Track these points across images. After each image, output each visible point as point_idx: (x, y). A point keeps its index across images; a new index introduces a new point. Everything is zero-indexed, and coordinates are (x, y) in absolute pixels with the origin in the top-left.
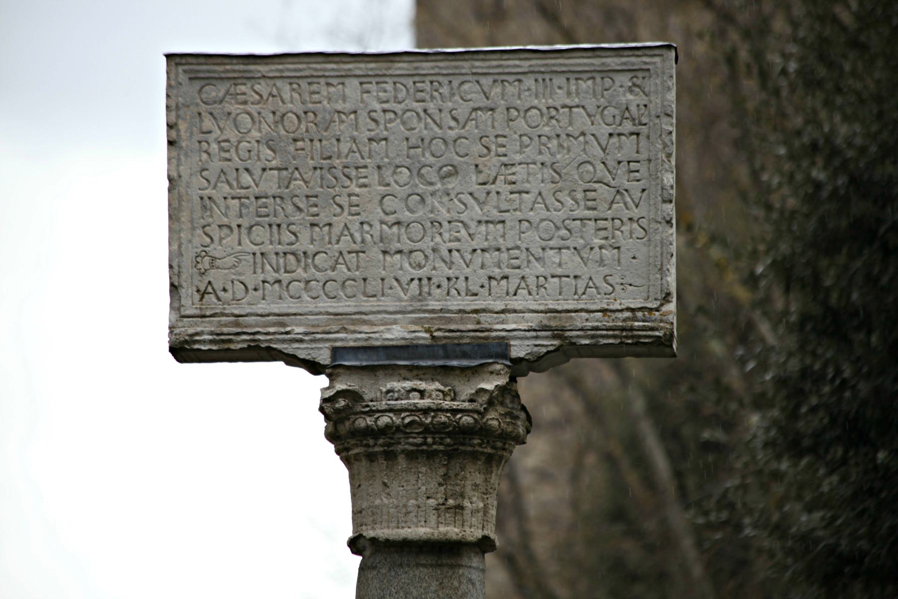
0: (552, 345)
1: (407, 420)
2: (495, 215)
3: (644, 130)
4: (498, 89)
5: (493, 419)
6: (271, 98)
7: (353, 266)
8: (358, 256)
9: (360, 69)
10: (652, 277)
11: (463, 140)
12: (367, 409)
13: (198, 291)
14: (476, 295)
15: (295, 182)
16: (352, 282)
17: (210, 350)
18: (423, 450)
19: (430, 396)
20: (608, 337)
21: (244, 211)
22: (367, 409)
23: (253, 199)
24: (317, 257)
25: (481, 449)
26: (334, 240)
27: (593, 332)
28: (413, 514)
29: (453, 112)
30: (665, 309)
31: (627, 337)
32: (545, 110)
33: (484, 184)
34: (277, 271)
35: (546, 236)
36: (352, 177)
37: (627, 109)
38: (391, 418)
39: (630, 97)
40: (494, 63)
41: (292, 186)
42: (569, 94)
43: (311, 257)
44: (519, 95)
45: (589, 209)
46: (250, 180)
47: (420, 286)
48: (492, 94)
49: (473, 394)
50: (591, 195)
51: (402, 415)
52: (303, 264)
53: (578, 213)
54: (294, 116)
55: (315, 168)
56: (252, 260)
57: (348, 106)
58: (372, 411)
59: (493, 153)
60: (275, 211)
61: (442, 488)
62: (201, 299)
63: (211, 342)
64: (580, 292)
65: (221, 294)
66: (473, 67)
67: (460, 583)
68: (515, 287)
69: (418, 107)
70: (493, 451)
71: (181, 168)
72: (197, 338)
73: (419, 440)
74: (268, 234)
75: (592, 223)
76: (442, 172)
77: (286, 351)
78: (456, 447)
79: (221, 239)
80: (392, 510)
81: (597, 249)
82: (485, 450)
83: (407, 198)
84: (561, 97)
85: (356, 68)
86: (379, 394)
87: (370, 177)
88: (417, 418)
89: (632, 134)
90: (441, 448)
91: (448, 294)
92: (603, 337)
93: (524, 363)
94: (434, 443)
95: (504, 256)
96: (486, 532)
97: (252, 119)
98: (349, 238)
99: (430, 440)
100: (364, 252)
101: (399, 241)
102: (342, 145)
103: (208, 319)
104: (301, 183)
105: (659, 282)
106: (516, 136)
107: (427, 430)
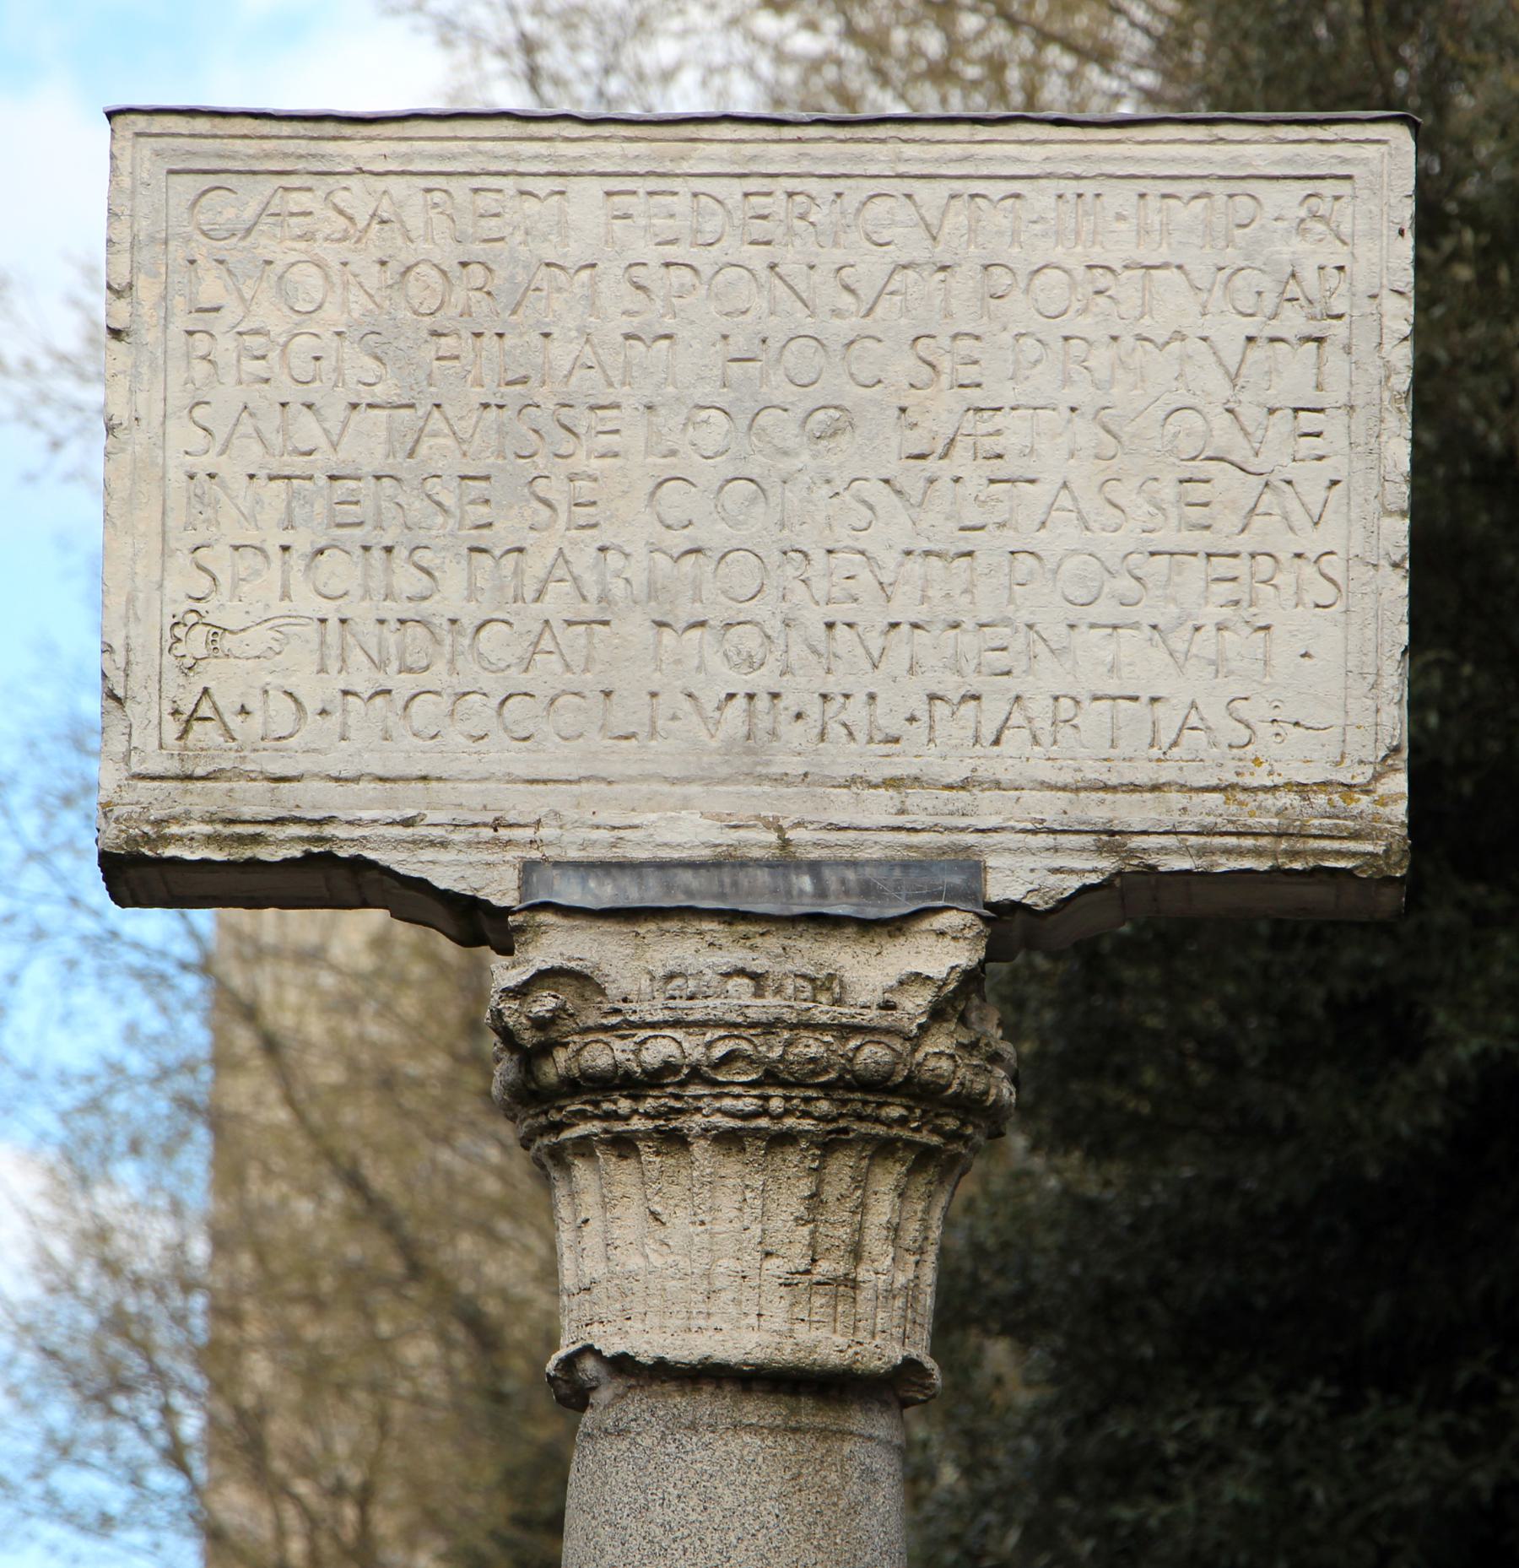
0: (1094, 870)
1: (719, 1051)
2: (947, 537)
3: (1338, 329)
4: (958, 217)
5: (940, 1054)
6: (375, 226)
7: (577, 661)
8: (590, 635)
9: (608, 157)
10: (1353, 705)
11: (869, 343)
12: (614, 1020)
13: (176, 712)
14: (897, 740)
15: (432, 441)
16: (577, 699)
17: (205, 863)
18: (758, 1129)
19: (778, 991)
20: (1240, 853)
21: (299, 512)
22: (614, 1020)
23: (322, 481)
24: (483, 633)
25: (905, 1134)
26: (529, 594)
27: (1202, 840)
28: (726, 1296)
29: (844, 272)
30: (1382, 788)
31: (1294, 854)
32: (1080, 272)
33: (922, 457)
34: (380, 665)
35: (1081, 595)
36: (581, 430)
37: (1293, 275)
38: (281, 1533)
39: (1298, 245)
40: (955, 150)
41: (423, 450)
42: (1143, 231)
43: (470, 630)
44: (1015, 233)
45: (1194, 527)
46: (318, 431)
47: (750, 714)
48: (946, 230)
49: (891, 990)
50: (1198, 492)
51: (708, 1037)
52: (447, 649)
53: (1159, 540)
54: (435, 273)
55: (486, 406)
56: (316, 639)
57: (575, 252)
58: (632, 1025)
59: (945, 380)
60: (379, 511)
61: (805, 1230)
62: (185, 732)
63: (210, 839)
64: (1166, 739)
65: (235, 722)
66: (899, 159)
67: (845, 1477)
68: (997, 724)
69: (757, 258)
70: (935, 1140)
71: (141, 397)
72: (174, 829)
73: (748, 1104)
74: (358, 572)
75: (1199, 563)
76: (812, 424)
77: (401, 870)
78: (842, 1123)
79: (237, 581)
80: (672, 1285)
81: (1209, 630)
82: (917, 1137)
83: (721, 488)
84: (1120, 246)
85: (597, 155)
86: (645, 982)
87: (625, 432)
88: (744, 1045)
89: (1309, 339)
90: (807, 1124)
91: (822, 736)
92: (1228, 852)
93: (1019, 917)
94: (787, 1112)
95: (968, 640)
96: (914, 1353)
97: (327, 277)
98: (567, 586)
99: (776, 1104)
100: (605, 623)
101: (697, 598)
102: (555, 348)
103: (199, 784)
104: (450, 442)
105: (1371, 720)
106: (1006, 338)
107: (771, 1077)
